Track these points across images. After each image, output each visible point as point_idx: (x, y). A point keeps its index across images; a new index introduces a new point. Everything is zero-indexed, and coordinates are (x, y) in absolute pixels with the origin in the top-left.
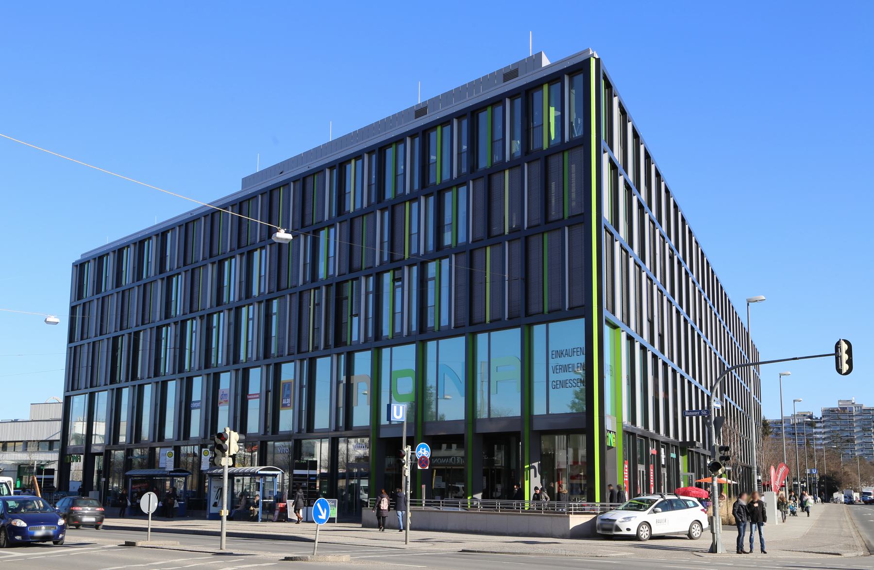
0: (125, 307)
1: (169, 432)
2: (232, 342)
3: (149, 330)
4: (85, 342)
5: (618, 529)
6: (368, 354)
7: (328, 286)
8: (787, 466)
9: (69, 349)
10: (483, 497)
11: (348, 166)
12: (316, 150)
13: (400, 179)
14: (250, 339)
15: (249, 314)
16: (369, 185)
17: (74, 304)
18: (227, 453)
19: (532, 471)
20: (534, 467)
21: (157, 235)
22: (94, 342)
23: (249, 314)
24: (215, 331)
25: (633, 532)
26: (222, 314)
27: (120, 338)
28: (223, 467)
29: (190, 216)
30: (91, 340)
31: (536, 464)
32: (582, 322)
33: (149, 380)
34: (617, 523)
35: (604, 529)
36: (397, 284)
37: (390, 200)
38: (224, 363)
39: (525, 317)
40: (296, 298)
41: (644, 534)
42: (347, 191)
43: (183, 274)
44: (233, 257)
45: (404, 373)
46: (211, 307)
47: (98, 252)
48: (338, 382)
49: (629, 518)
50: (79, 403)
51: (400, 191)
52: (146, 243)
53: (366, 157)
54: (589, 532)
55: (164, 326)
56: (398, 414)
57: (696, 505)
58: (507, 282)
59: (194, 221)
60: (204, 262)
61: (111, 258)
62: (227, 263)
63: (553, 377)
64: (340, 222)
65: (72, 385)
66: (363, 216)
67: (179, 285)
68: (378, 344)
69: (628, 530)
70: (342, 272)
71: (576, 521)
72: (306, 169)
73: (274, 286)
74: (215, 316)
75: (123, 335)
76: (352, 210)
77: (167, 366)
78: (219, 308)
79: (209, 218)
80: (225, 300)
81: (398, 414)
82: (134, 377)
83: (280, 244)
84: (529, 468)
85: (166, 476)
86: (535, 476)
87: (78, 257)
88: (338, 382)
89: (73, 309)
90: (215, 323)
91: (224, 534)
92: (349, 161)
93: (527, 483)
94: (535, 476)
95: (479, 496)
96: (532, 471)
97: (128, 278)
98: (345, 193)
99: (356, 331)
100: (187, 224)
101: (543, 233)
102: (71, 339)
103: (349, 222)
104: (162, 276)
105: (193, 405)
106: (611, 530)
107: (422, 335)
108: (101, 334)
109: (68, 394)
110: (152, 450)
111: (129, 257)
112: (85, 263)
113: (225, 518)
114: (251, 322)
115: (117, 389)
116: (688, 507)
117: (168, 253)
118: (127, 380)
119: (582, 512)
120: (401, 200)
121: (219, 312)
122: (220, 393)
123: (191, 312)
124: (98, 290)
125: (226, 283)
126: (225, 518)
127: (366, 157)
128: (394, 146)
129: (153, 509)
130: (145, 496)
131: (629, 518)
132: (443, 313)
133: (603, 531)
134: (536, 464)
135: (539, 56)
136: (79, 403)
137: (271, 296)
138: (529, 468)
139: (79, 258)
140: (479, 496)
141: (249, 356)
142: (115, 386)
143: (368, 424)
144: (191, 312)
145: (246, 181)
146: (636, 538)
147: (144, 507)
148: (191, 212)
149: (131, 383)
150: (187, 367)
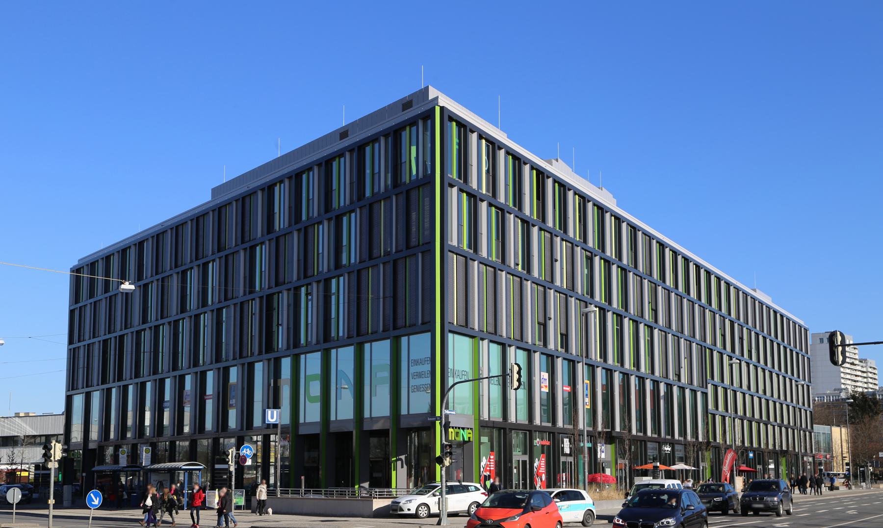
0: (117, 312)
1: (209, 425)
2: (291, 326)
3: (232, 307)
4: (112, 335)
5: (402, 510)
6: (318, 355)
7: (261, 298)
8: (734, 451)
9: (69, 350)
10: (370, 486)
11: (403, 133)
12: (362, 120)
13: (376, 177)
14: (310, 322)
15: (340, 287)
16: (351, 183)
17: (72, 308)
18: (52, 458)
19: (399, 463)
20: (401, 460)
21: (290, 178)
22: (89, 345)
23: (340, 287)
24: (333, 298)
25: (413, 511)
26: (341, 279)
27: (276, 297)
28: (50, 469)
29: (161, 227)
30: (171, 319)
31: (403, 457)
32: (428, 335)
33: (235, 362)
34: (401, 504)
35: (393, 510)
36: (310, 297)
37: (368, 198)
38: (285, 347)
39: (396, 328)
40: (389, 268)
41: (423, 512)
42: (403, 161)
43: (267, 242)
44: (353, 211)
45: (313, 377)
46: (329, 270)
47: (90, 258)
48: (269, 385)
49: (410, 501)
50: (78, 401)
51: (376, 190)
52: (304, 176)
53: (382, 140)
54: (383, 513)
55: (142, 330)
56: (272, 418)
57: (477, 489)
58: (381, 300)
59: (250, 195)
60: (237, 248)
61: (133, 250)
62: (345, 219)
63: (413, 382)
64: (396, 195)
65: (72, 385)
66: (419, 187)
67: (262, 255)
68: (297, 351)
69: (409, 510)
70: (399, 249)
71: (378, 504)
72: (243, 190)
73: (365, 256)
74: (334, 281)
75: (183, 319)
76: (408, 181)
77: (184, 360)
78: (338, 272)
79: (216, 213)
80: (344, 261)
81: (272, 418)
82: (196, 364)
83: (127, 294)
84: (396, 461)
85: (120, 471)
86: (402, 467)
87: (75, 263)
88: (269, 385)
89: (72, 312)
90: (334, 290)
91: (51, 517)
92: (404, 128)
93: (394, 473)
94: (402, 467)
95: (366, 485)
96: (399, 463)
97: (281, 221)
98: (401, 164)
99: (281, 340)
100: (243, 198)
101: (406, 257)
102: (71, 341)
103: (369, 209)
104: (270, 236)
105: (165, 404)
106: (396, 510)
107: (326, 343)
108: (162, 318)
109: (69, 393)
110: (216, 441)
111: (282, 196)
112: (143, 241)
113: (51, 507)
114: (310, 303)
115: (224, 368)
116: (468, 491)
117: (276, 210)
118: (260, 353)
119: (381, 497)
120: (377, 199)
121: (339, 276)
122: (185, 394)
123: (277, 285)
124: (91, 295)
125: (345, 242)
126: (51, 507)
127: (382, 140)
128: (337, 159)
129: (17, 501)
130: (11, 491)
131: (410, 501)
132: (340, 326)
133: (393, 512)
134: (403, 457)
135: (427, 89)
136: (78, 401)
137: (300, 283)
138: (396, 461)
139: (76, 263)
140: (366, 485)
141: (309, 339)
142: (177, 373)
143: (352, 417)
144: (277, 285)
145: (215, 191)
146: (416, 516)
147: (10, 499)
148: (162, 224)
149: (239, 361)
150: (303, 341)
